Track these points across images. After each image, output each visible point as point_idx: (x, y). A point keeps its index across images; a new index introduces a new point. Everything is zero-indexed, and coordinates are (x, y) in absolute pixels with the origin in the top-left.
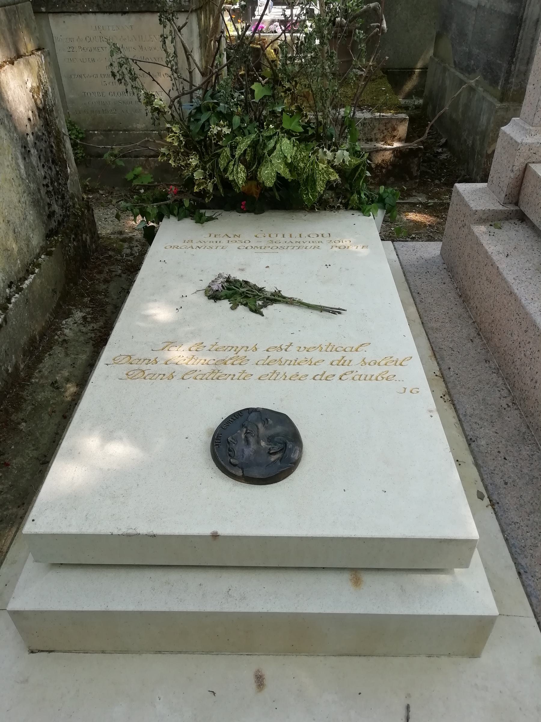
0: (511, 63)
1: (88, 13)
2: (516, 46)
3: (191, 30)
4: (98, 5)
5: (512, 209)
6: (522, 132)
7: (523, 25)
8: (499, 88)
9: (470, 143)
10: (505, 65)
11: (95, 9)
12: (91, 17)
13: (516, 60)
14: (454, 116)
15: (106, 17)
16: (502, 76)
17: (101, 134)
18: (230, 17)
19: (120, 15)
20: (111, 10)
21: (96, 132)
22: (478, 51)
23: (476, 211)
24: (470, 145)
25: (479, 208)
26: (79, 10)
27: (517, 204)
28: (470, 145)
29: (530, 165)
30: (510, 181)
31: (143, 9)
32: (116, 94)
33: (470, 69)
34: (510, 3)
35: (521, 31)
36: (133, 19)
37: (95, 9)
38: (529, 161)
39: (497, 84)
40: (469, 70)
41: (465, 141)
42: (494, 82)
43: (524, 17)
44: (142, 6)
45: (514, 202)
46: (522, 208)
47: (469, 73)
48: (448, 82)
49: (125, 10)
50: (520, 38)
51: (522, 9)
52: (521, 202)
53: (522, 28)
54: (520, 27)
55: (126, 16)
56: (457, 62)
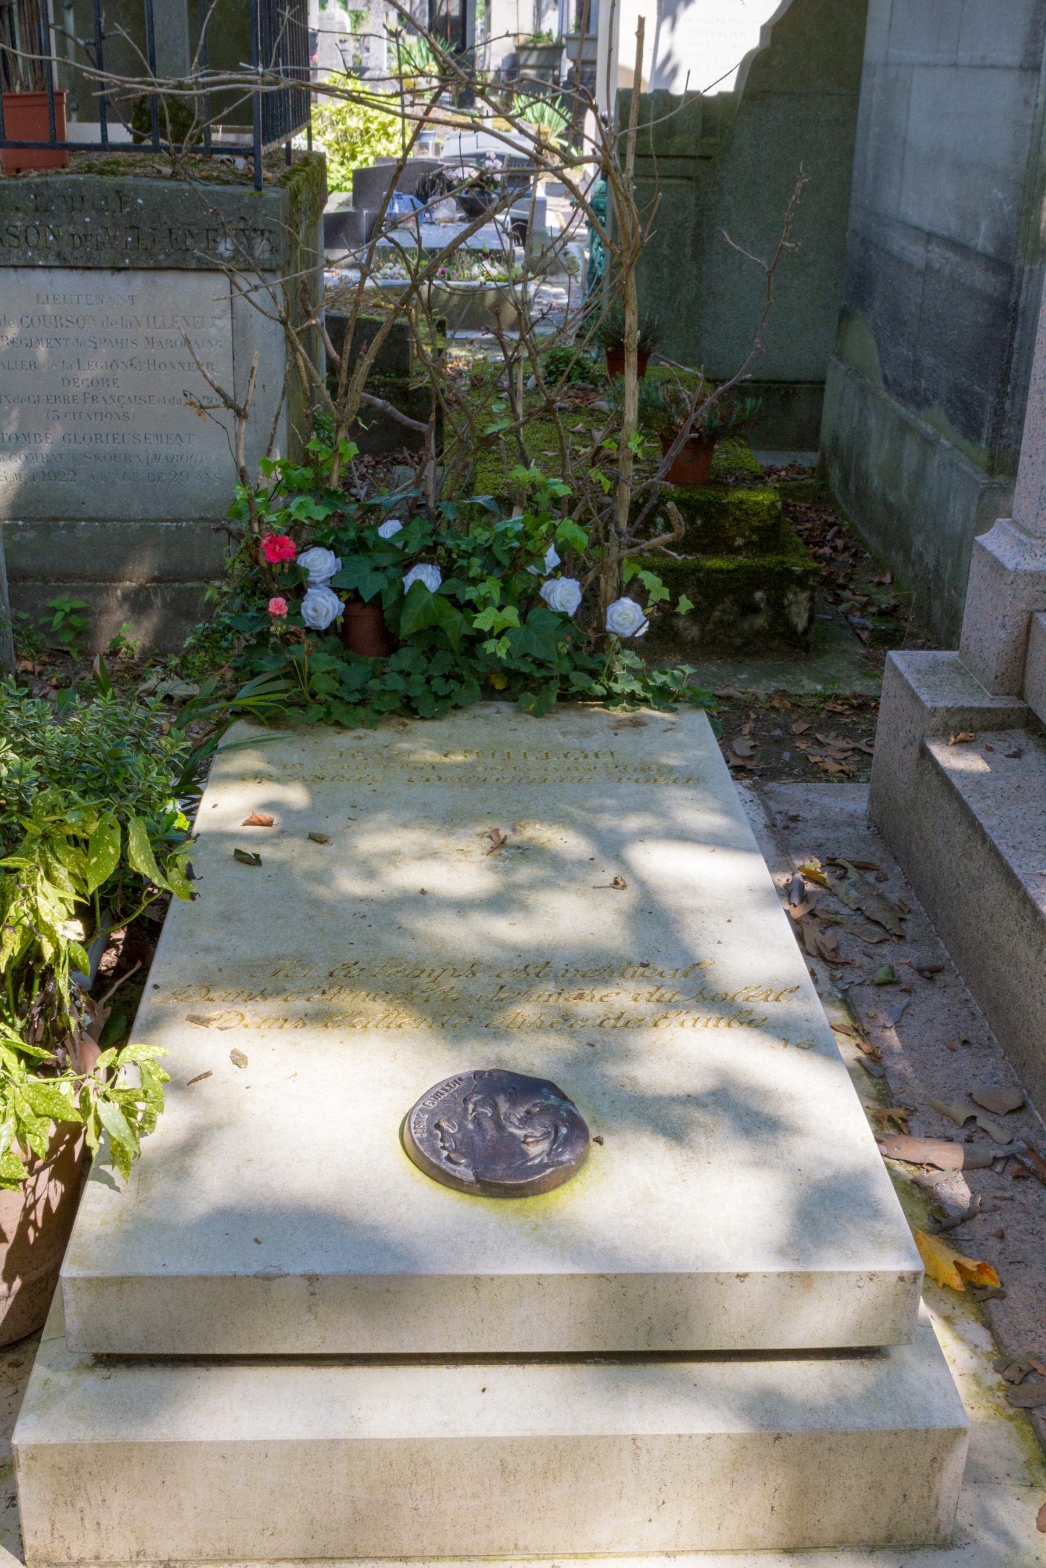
0: (1001, 395)
1: (34, 267)
2: (1009, 361)
3: (264, 295)
4: (59, 255)
5: (1011, 706)
6: (1016, 549)
7: (1020, 320)
8: (983, 445)
9: (930, 560)
10: (991, 398)
11: (52, 261)
12: (40, 277)
13: (1013, 388)
14: (891, 498)
15: (75, 276)
16: (987, 419)
17: (33, 527)
18: (992, 1301)
19: (107, 274)
20: (90, 264)
21: (20, 523)
22: (933, 360)
23: (935, 709)
24: (931, 566)
25: (941, 704)
26: (14, 261)
27: (1021, 695)
28: (931, 566)
29: (1038, 615)
30: (1001, 646)
31: (165, 264)
32: (79, 439)
33: (919, 398)
34: (990, 273)
35: (1018, 333)
36: (138, 281)
37: (52, 261)
38: (1035, 607)
39: (979, 437)
40: (918, 399)
41: (920, 556)
42: (971, 430)
43: (1021, 306)
44: (162, 257)
45: (1016, 690)
46: (1031, 704)
47: (919, 406)
48: (873, 421)
49: (122, 265)
50: (1016, 345)
51: (1014, 289)
52: (1027, 693)
53: (1019, 325)
54: (1015, 322)
55: (122, 277)
56: (890, 378)
